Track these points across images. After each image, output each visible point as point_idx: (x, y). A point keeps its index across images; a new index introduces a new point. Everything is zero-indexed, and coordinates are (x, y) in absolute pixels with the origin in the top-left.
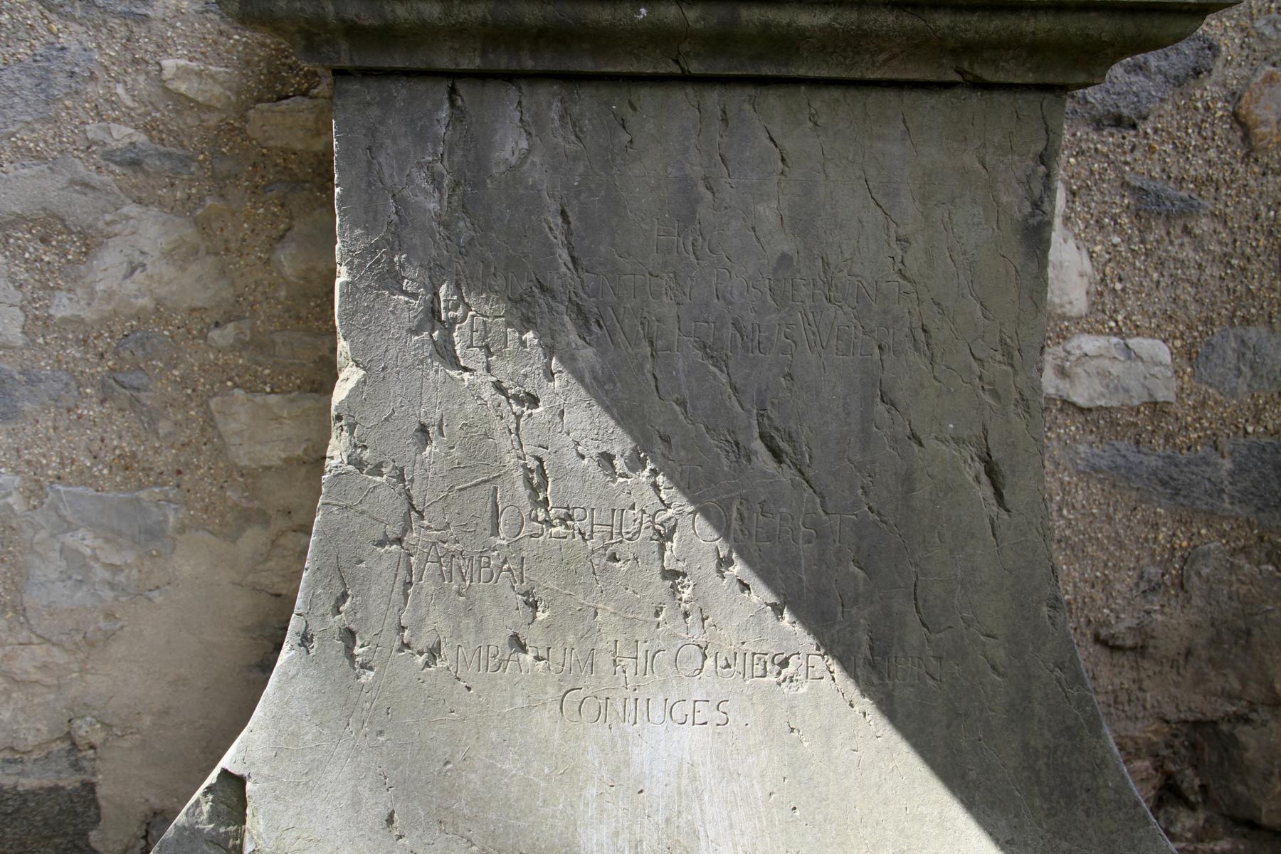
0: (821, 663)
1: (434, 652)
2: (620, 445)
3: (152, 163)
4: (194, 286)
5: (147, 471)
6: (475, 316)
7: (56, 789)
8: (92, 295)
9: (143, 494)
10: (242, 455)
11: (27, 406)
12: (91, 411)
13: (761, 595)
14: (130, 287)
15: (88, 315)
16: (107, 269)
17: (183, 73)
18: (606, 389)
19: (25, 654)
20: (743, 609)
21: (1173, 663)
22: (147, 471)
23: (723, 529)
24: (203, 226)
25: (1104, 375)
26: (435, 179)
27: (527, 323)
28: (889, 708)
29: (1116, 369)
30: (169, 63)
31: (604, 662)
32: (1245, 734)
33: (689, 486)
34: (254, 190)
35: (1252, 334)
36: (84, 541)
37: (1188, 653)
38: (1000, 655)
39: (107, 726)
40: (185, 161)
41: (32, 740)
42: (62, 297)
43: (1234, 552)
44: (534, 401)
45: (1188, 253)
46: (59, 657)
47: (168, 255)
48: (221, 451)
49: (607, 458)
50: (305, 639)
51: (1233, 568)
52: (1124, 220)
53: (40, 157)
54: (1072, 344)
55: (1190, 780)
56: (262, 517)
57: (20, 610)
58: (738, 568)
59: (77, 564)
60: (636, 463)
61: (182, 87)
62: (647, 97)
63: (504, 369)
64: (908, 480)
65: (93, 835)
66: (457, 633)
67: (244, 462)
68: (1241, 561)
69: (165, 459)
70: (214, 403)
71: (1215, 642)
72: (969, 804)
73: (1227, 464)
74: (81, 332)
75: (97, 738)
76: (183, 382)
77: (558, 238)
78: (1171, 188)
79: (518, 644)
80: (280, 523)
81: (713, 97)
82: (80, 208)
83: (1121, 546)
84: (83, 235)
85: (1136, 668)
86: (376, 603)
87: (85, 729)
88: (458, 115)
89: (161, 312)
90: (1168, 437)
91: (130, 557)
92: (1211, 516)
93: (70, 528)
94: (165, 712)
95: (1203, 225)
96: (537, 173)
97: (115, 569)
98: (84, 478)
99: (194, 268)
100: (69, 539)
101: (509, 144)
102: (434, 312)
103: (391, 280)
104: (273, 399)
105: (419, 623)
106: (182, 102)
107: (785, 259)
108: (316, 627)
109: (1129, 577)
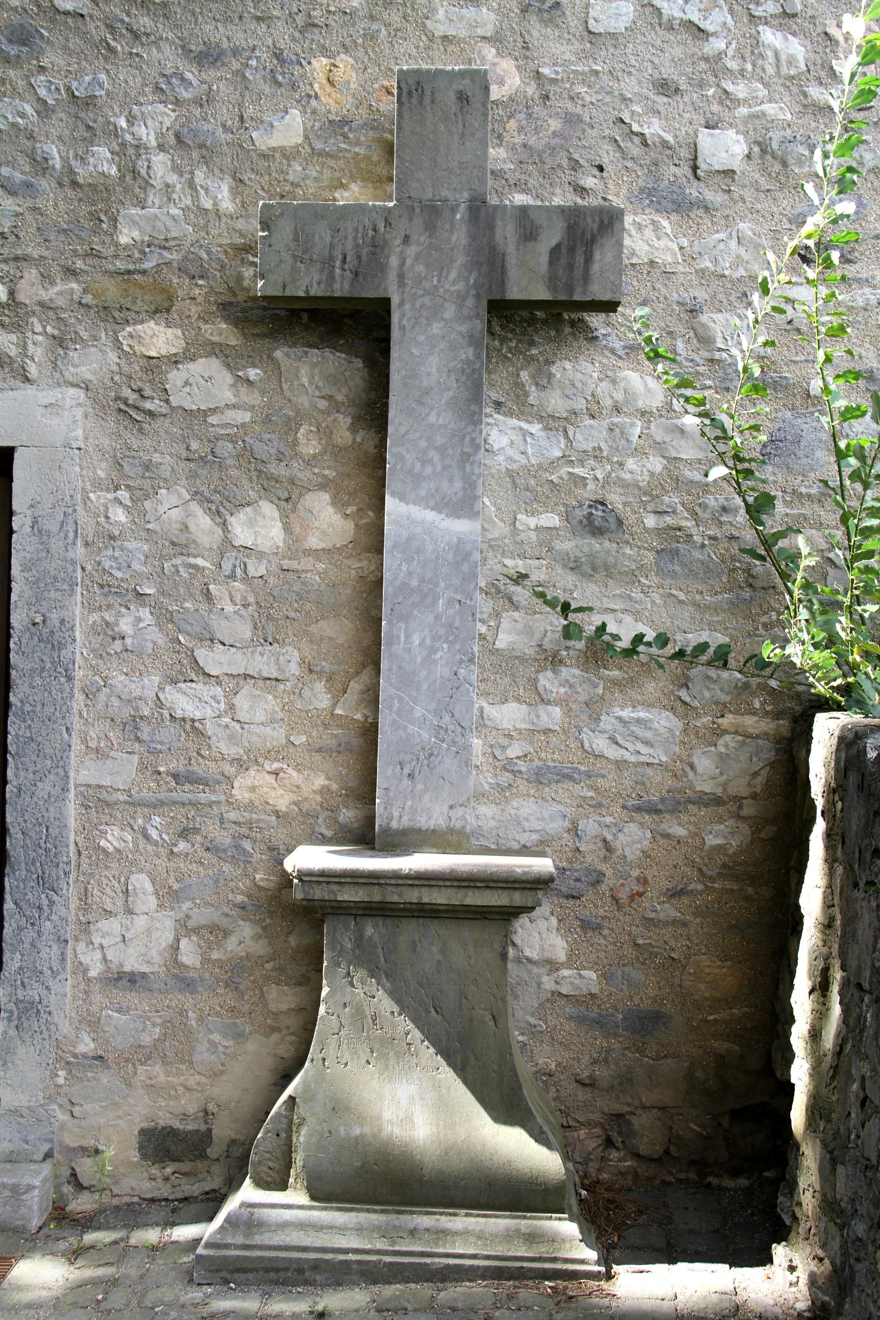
0: (447, 1068)
1: (346, 1064)
2: (396, 1009)
3: (249, 908)
4: (260, 948)
5: (239, 1012)
6: (359, 974)
7: (198, 1131)
8: (226, 951)
9: (238, 1021)
10: (273, 1007)
11: (200, 989)
12: (221, 991)
13: (432, 1050)
14: (239, 949)
15: (223, 958)
16: (232, 943)
17: (262, 879)
18: (395, 995)
19: (192, 1078)
20: (427, 1053)
21: (607, 1091)
22: (239, 1012)
23: (422, 1032)
24: (265, 929)
25: (572, 983)
26: (350, 939)
27: (373, 977)
28: (465, 1082)
29: (576, 982)
30: (257, 876)
31: (391, 1067)
32: (634, 1119)
33: (414, 1020)
34: (283, 917)
35: (626, 969)
36: (216, 1037)
37: (612, 1087)
38: (496, 1068)
39: (219, 1106)
40: (260, 907)
41: (192, 1111)
42: (215, 952)
43: (624, 1049)
44: (374, 997)
45: (602, 941)
46: (204, 1080)
47: (252, 938)
48: (265, 1005)
49: (393, 1013)
50: (312, 1060)
51: (624, 1055)
52: (578, 929)
53: (213, 906)
54: (560, 973)
55: (617, 1139)
56: (279, 1030)
57: (191, 1063)
58: (426, 1043)
59: (213, 1044)
60: (400, 1014)
61: (261, 884)
62: (404, 920)
63: (366, 989)
64: (471, 1020)
65: (208, 1150)
66: (352, 1059)
67: (274, 1010)
68: (627, 1052)
69: (246, 1008)
70: (265, 989)
71: (621, 1084)
72: (486, 1109)
73: (620, 1016)
74: (220, 964)
75: (215, 1110)
76: (254, 981)
77: (381, 955)
78: (593, 919)
79: (368, 1062)
80: (285, 1032)
81: (421, 920)
82: (224, 922)
83: (583, 1046)
84: (224, 931)
85: (592, 1092)
86: (331, 1052)
87: (211, 1107)
88: (356, 924)
89: (248, 957)
90: (599, 1006)
91: (231, 1043)
92: (615, 1035)
93: (211, 1032)
94: (239, 1102)
95: (606, 932)
96: (376, 938)
97: (226, 1047)
98: (218, 1014)
99: (261, 942)
100: (211, 1037)
101: (369, 931)
102: (349, 973)
103: (338, 965)
104: (285, 988)
105: (342, 1056)
106: (260, 888)
107: (439, 961)
108: (315, 1057)
109: (587, 1057)
